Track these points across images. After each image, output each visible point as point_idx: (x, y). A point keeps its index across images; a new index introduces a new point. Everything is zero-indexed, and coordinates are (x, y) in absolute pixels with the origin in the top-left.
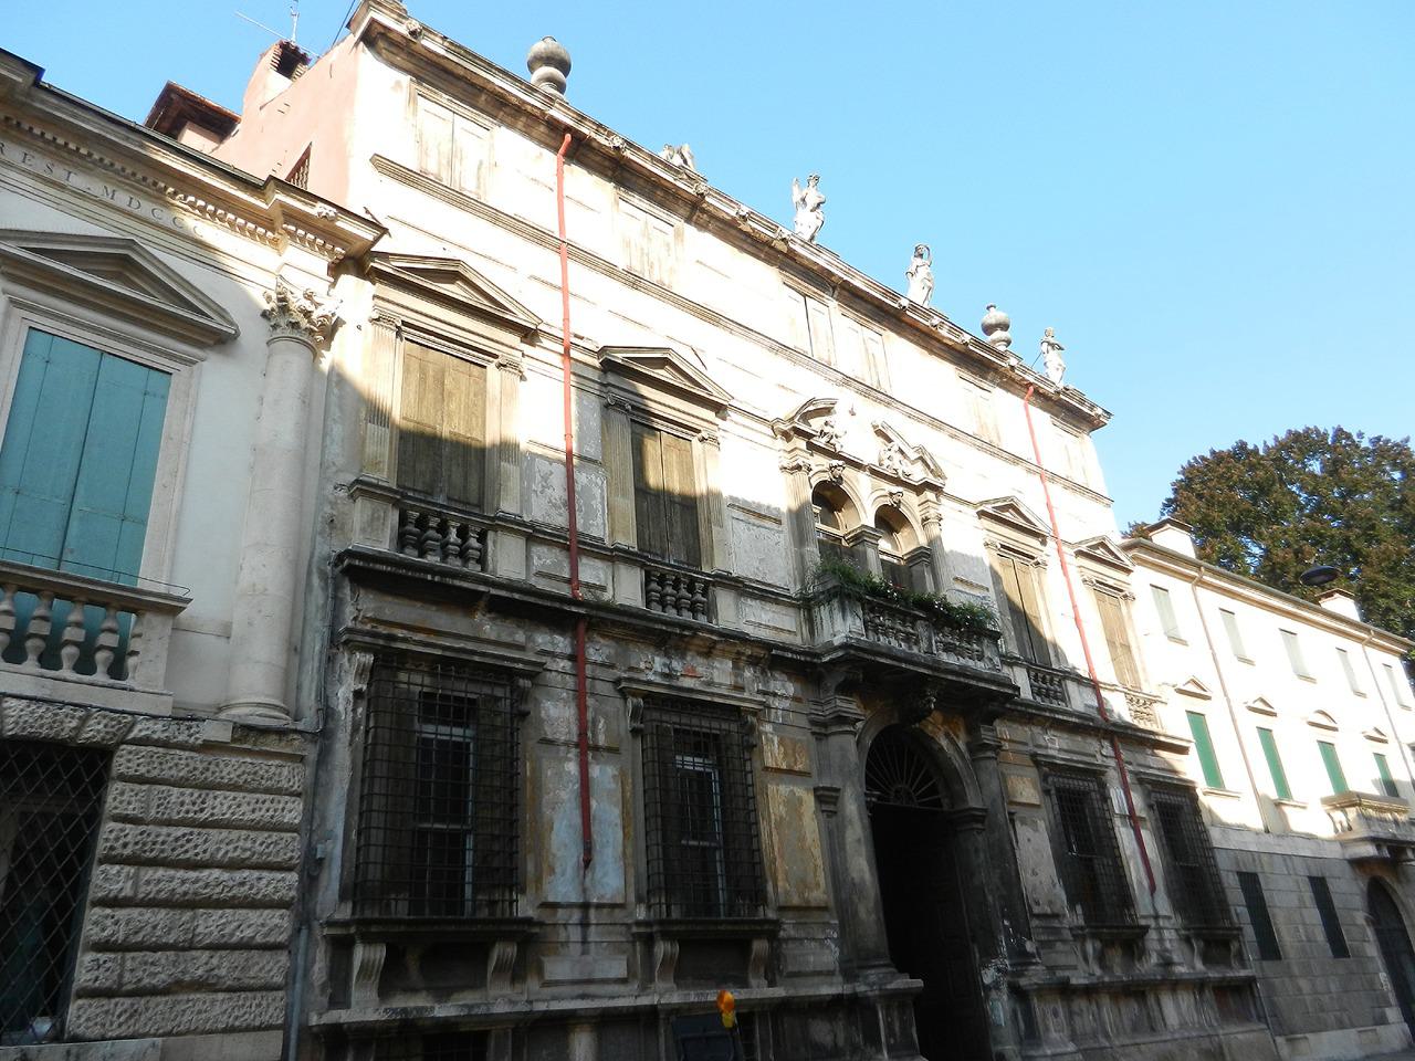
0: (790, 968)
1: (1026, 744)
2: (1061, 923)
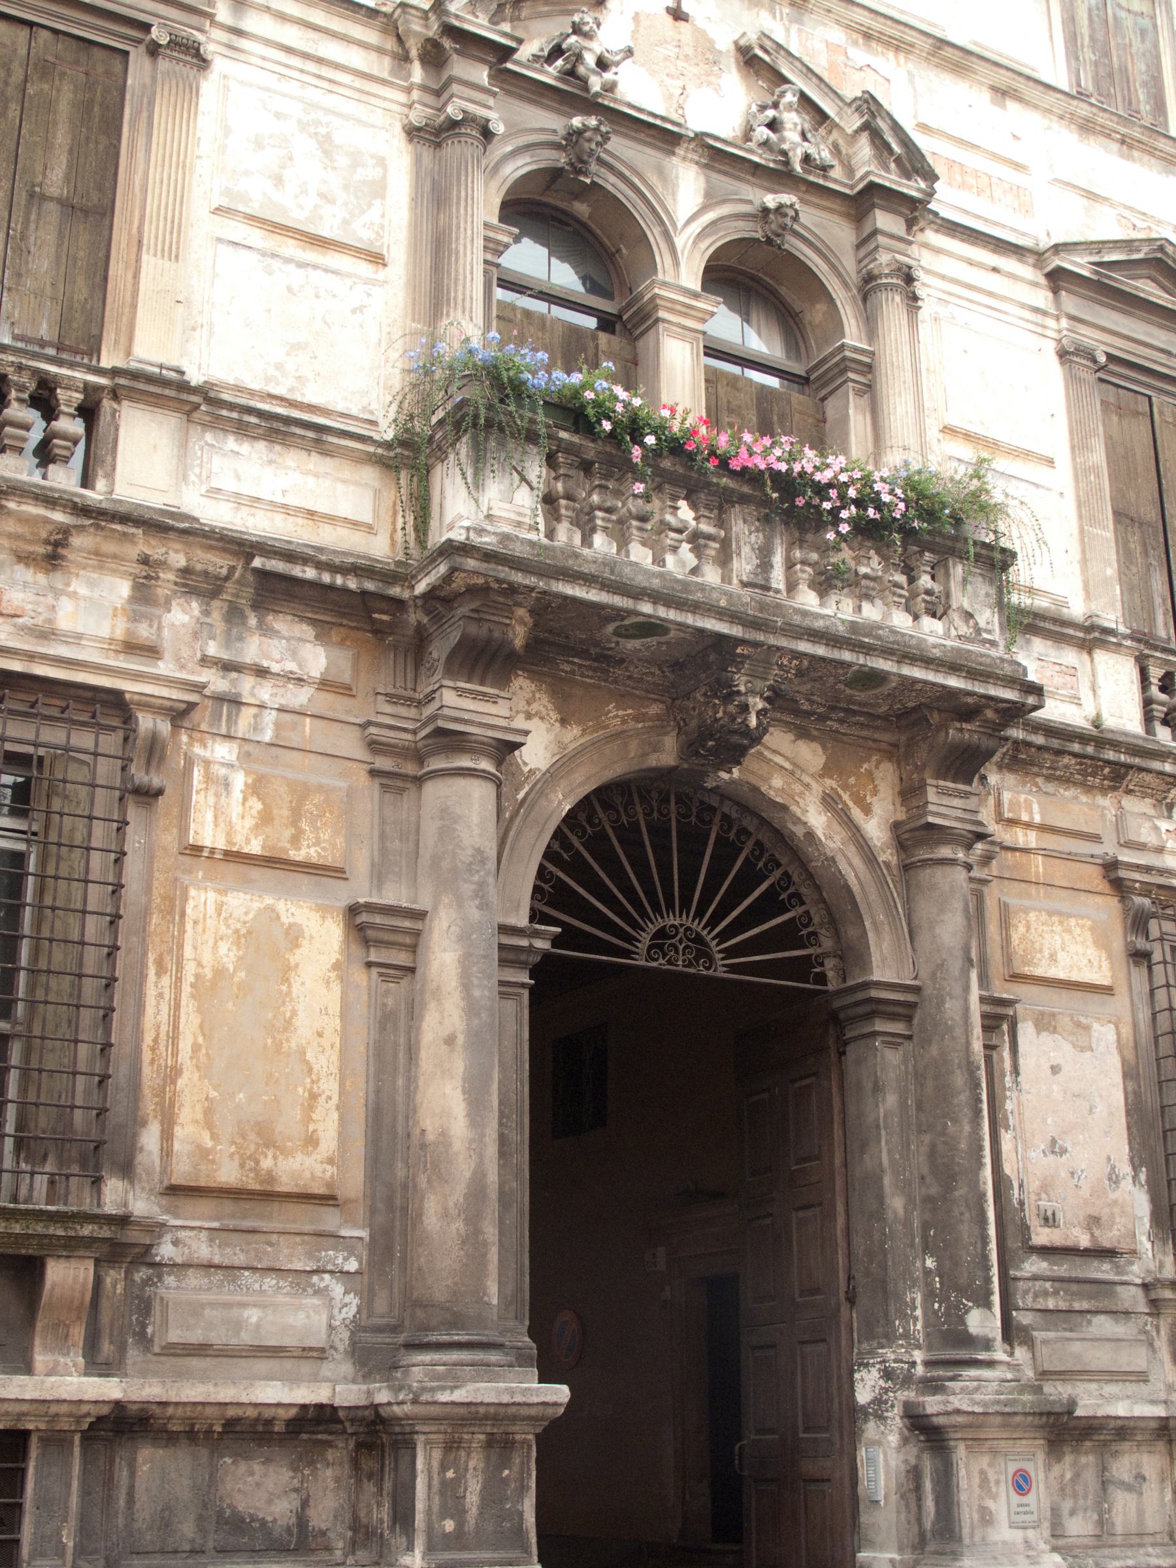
0: (175, 1335)
1: (1095, 838)
2: (1119, 1270)
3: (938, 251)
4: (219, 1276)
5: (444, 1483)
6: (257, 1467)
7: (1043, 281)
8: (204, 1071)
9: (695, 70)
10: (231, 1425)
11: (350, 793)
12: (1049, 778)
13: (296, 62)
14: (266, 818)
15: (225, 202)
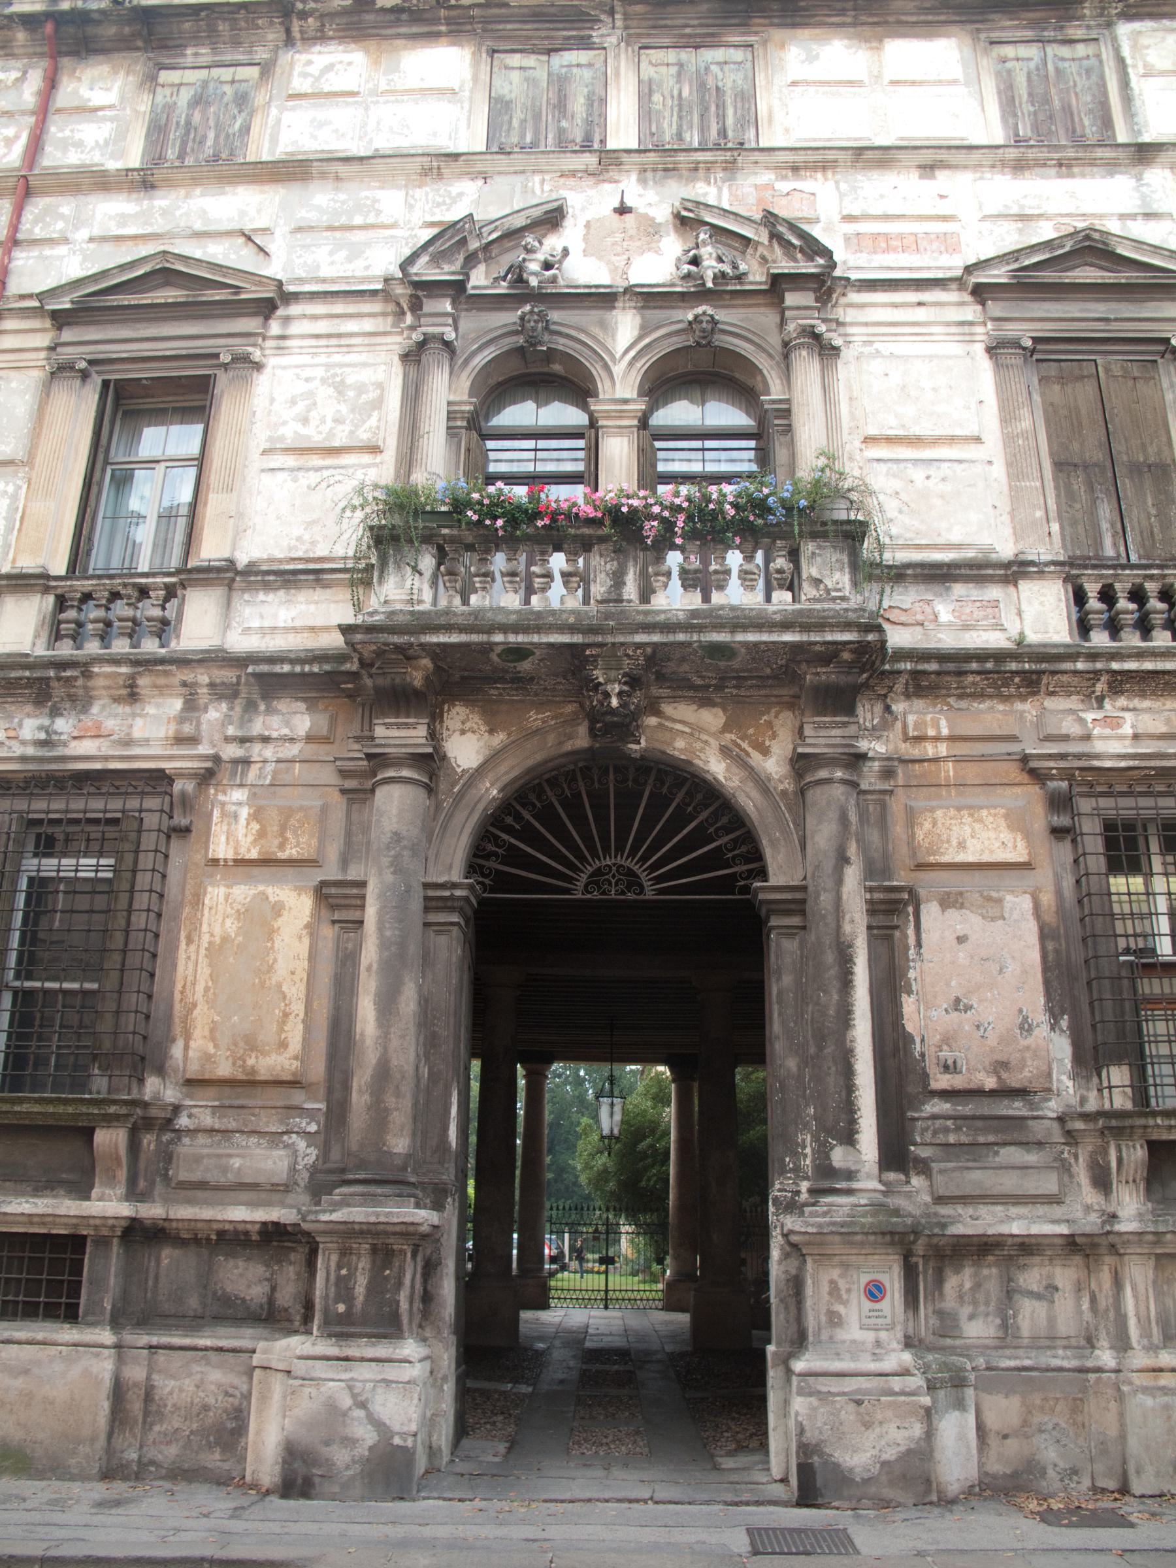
0: (183, 1176)
1: (1013, 738)
2: (1032, 1106)
3: (863, 306)
4: (218, 1137)
5: (339, 1279)
6: (241, 1263)
7: (968, 298)
8: (211, 1004)
9: (638, 244)
10: (221, 1234)
11: (324, 809)
12: (961, 697)
13: (323, 342)
14: (262, 834)
15: (267, 446)
